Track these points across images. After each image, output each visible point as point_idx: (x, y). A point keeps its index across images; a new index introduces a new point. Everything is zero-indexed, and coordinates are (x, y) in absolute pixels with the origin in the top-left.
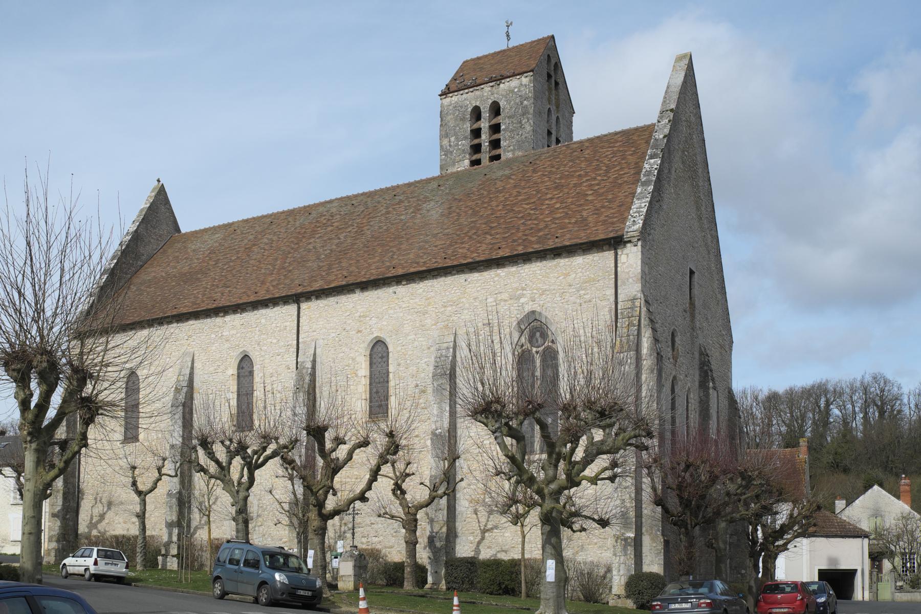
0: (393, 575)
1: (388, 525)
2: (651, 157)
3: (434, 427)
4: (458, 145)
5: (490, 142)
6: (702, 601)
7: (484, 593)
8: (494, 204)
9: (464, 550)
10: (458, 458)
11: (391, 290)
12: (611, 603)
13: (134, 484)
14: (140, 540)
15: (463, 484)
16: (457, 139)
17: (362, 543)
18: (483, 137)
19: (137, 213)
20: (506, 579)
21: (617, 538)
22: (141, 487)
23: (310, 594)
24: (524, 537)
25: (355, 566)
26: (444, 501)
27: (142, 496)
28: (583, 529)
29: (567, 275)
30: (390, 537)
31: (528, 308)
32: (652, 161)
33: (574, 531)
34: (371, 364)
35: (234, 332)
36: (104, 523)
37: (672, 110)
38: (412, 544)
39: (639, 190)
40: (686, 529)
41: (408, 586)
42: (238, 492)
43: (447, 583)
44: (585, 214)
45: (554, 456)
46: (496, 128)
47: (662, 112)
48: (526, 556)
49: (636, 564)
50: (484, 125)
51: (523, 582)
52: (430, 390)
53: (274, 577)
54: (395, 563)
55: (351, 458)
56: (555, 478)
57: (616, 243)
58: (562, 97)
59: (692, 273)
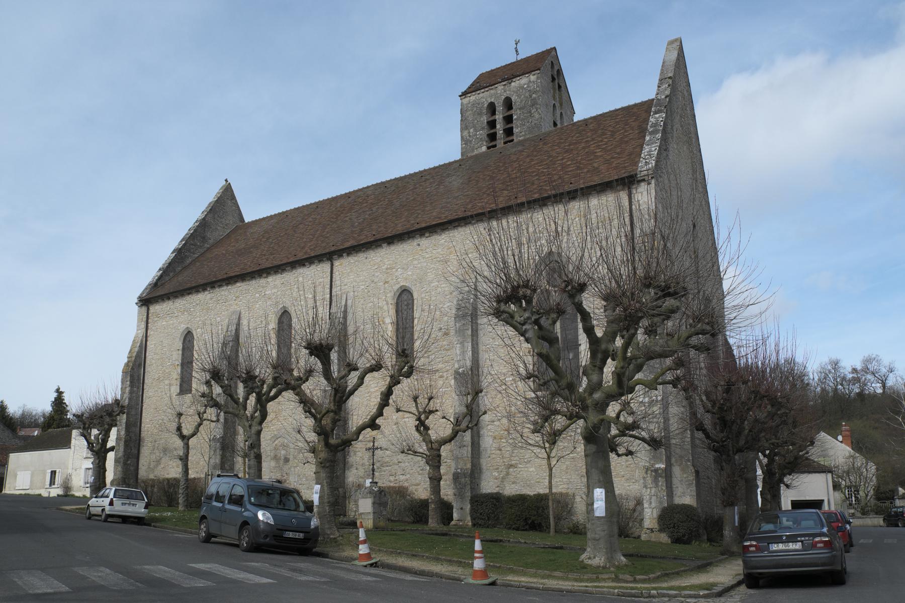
0: (418, 512)
1: (415, 463)
2: (656, 113)
3: (456, 366)
4: (476, 135)
5: (504, 130)
6: (817, 539)
7: (510, 528)
8: (510, 169)
9: (488, 486)
10: (481, 391)
11: (415, 242)
12: (644, 537)
13: (179, 429)
14: (182, 483)
15: (486, 418)
16: (476, 130)
17: (390, 481)
18: (498, 126)
19: (206, 205)
20: (531, 516)
21: (647, 470)
22: (185, 432)
23: (301, 536)
24: (551, 469)
25: (374, 503)
26: (468, 436)
27: (186, 441)
28: (630, 453)
30: (416, 475)
32: (657, 116)
33: (619, 455)
34: (397, 311)
35: (275, 291)
36: (160, 468)
37: (670, 78)
38: (435, 480)
39: (647, 138)
40: (729, 456)
41: (433, 523)
42: (250, 426)
43: (473, 519)
44: (596, 165)
45: (600, 356)
46: (509, 119)
47: (661, 80)
48: (554, 490)
49: (668, 496)
50: (499, 117)
51: (551, 517)
52: (452, 332)
53: (256, 516)
54: (421, 500)
55: (362, 383)
56: (600, 384)
57: (629, 182)
58: (564, 98)
59: (53, 473)
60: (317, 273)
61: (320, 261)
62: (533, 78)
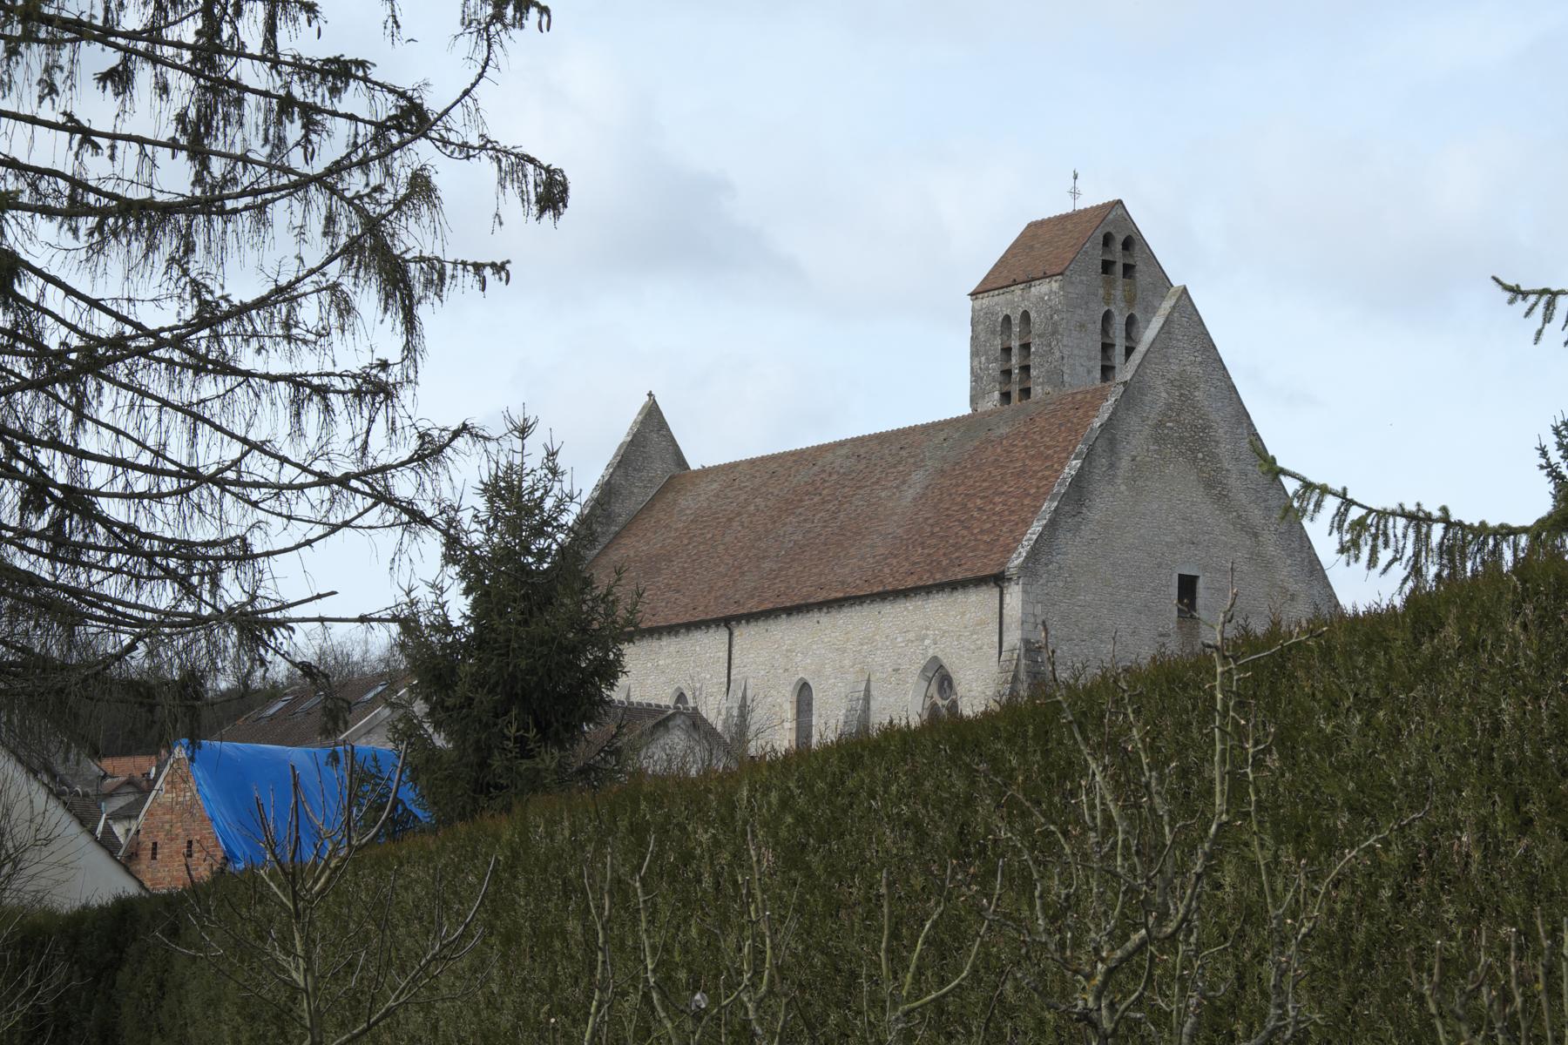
19: (614, 450)
29: (963, 614)
31: (931, 653)
57: (999, 580)
59: (1187, 586)
60: (711, 643)
61: (718, 626)
62: (1055, 286)
